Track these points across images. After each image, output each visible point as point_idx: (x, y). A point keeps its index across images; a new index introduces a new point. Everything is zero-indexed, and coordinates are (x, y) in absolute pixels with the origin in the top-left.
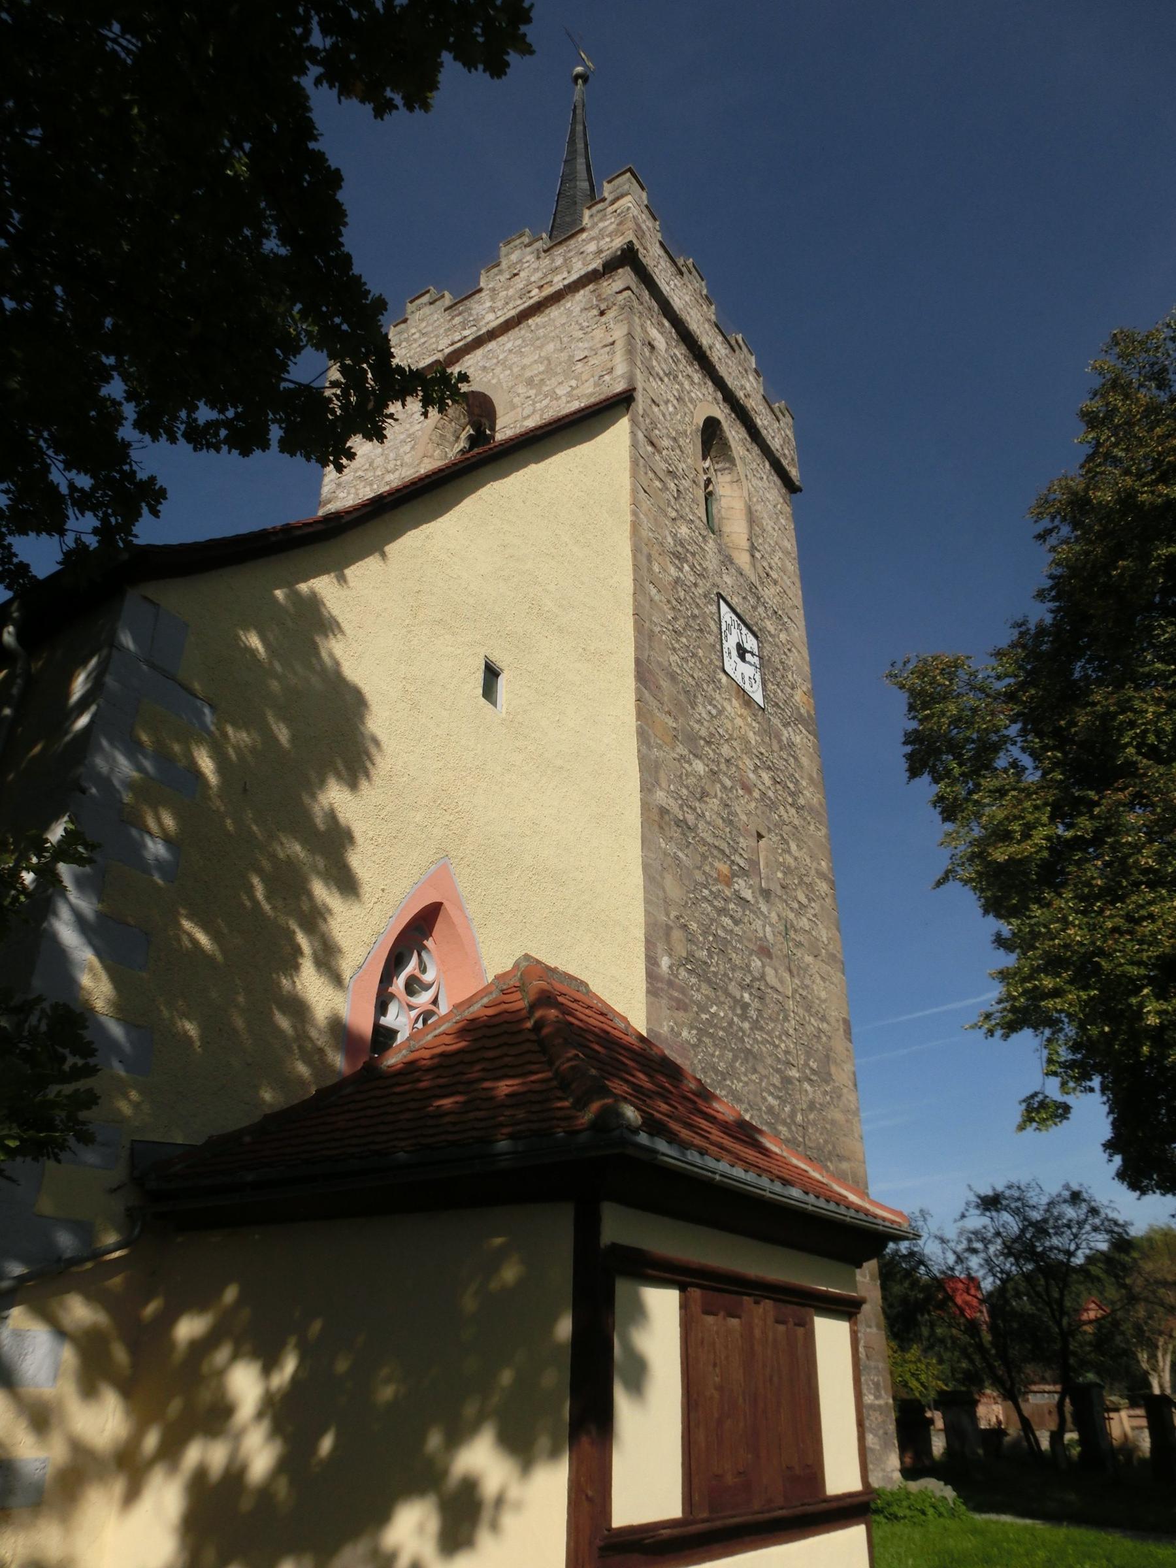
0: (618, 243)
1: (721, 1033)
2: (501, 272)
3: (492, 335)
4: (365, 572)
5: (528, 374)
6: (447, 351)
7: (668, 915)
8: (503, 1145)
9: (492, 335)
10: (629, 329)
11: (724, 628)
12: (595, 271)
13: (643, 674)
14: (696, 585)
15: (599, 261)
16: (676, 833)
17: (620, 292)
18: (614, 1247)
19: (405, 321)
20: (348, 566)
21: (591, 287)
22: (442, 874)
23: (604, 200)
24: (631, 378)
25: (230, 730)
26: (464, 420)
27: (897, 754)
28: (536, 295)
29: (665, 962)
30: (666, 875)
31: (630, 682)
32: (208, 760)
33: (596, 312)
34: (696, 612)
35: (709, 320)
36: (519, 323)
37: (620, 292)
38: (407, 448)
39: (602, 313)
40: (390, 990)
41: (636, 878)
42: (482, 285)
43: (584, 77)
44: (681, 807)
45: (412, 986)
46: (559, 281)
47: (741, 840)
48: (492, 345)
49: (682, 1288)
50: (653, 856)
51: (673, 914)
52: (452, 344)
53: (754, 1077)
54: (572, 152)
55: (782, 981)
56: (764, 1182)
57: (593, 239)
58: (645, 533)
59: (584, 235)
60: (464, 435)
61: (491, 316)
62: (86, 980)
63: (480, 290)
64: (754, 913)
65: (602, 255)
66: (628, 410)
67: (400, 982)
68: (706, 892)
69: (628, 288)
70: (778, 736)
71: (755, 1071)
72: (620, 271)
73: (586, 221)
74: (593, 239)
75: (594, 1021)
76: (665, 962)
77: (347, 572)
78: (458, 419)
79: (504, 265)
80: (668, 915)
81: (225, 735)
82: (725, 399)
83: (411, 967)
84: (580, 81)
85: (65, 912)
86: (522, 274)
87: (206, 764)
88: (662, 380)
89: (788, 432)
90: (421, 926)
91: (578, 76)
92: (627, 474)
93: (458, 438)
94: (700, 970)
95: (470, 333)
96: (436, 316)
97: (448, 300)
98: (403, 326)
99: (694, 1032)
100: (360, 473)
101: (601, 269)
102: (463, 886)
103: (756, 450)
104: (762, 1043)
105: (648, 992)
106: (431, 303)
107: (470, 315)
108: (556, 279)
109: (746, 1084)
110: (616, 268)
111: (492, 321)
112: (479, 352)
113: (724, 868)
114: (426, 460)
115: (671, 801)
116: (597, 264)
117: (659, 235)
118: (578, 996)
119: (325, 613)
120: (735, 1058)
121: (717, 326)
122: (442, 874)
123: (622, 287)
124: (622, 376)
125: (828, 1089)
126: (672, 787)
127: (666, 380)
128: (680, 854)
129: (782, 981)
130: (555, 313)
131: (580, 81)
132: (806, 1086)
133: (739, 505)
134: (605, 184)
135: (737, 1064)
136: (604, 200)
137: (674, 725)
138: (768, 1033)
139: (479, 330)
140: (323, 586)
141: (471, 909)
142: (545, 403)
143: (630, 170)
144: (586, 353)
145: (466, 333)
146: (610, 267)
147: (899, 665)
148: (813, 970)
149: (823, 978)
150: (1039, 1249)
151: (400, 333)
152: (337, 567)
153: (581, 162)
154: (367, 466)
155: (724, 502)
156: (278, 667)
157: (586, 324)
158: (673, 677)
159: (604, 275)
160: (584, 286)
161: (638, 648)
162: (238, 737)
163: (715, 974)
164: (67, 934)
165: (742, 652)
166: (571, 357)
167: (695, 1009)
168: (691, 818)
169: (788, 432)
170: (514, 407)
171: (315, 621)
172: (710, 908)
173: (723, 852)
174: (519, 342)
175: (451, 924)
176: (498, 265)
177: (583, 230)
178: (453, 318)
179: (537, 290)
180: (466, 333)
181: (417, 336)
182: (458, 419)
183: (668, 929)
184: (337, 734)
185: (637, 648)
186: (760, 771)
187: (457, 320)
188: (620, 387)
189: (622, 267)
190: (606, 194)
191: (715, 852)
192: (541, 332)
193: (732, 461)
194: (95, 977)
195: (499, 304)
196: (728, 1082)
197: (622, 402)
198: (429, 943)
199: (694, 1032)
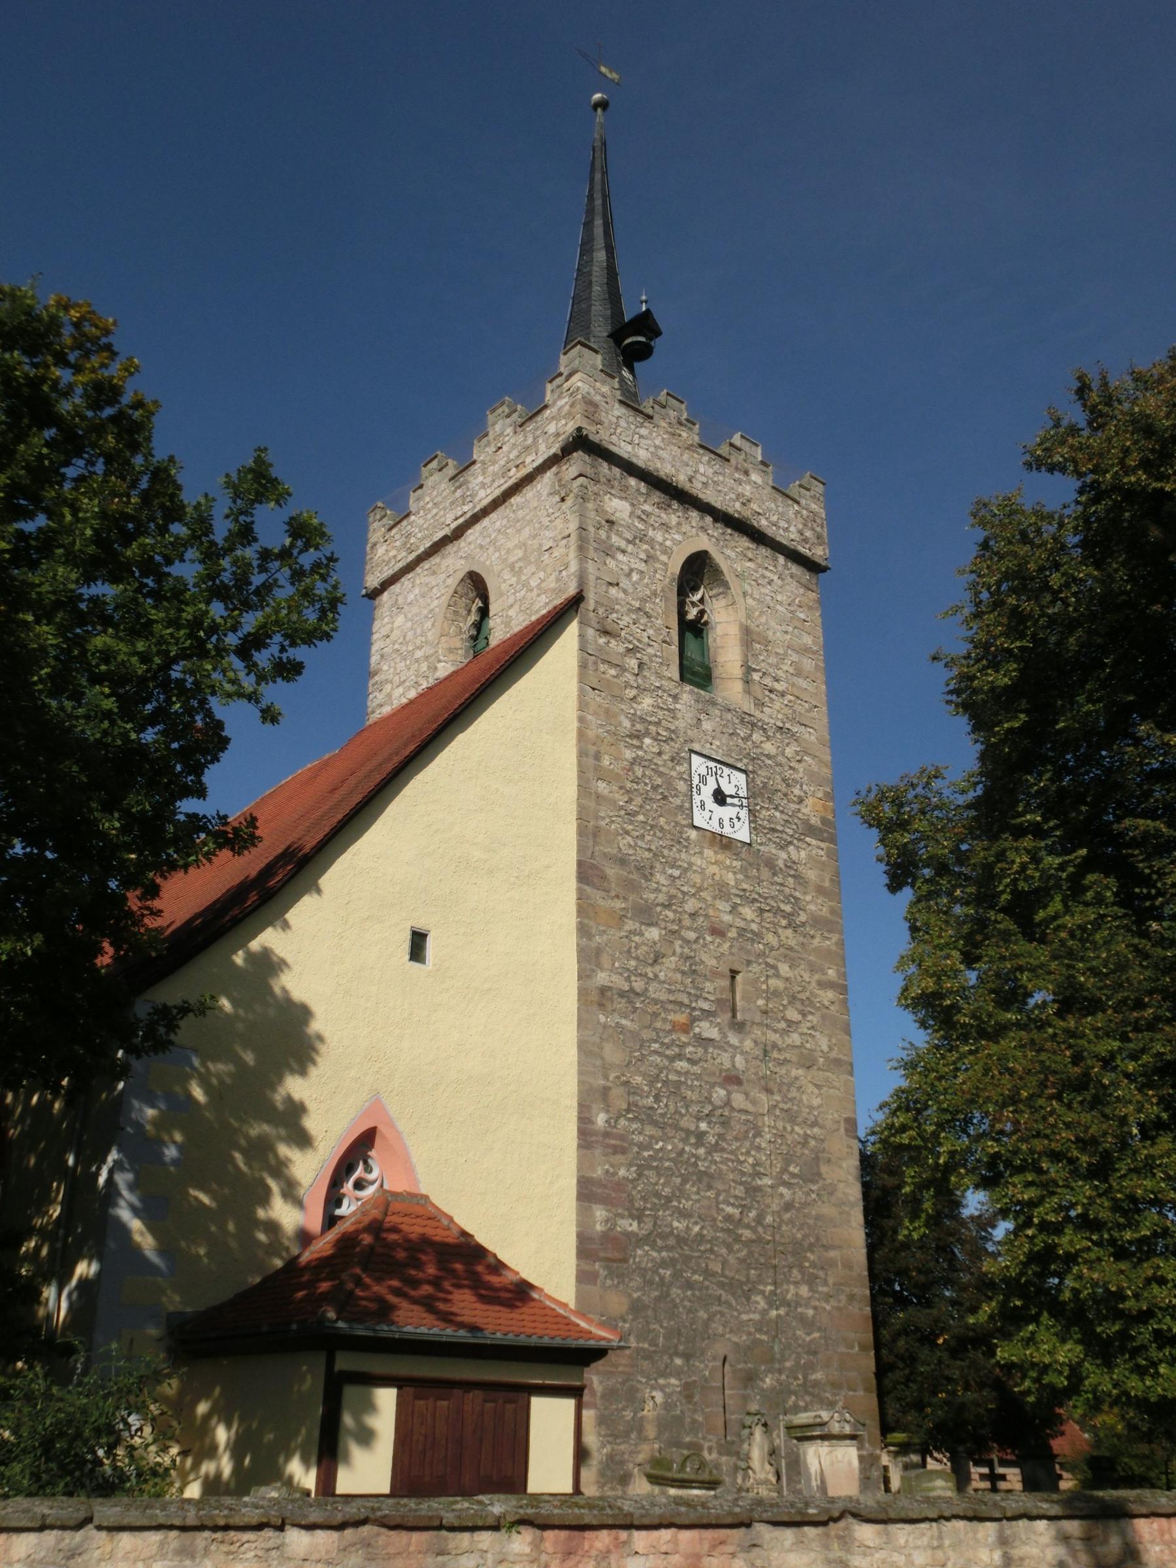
0: (570, 428)
1: (667, 1164)
2: (488, 444)
3: (485, 512)
4: (304, 912)
5: (512, 559)
6: (453, 526)
7: (606, 1077)
8: (294, 1327)
9: (485, 512)
10: (581, 522)
11: (696, 781)
12: (555, 455)
13: (587, 873)
14: (660, 754)
15: (557, 445)
16: (621, 1004)
17: (575, 478)
18: (341, 1372)
19: (421, 487)
20: (287, 911)
21: (554, 469)
22: (376, 1105)
23: (561, 374)
24: (582, 578)
25: (210, 1065)
26: (472, 595)
27: (879, 875)
28: (516, 475)
29: (601, 1119)
30: (605, 1044)
31: (572, 884)
32: (198, 1090)
33: (557, 498)
34: (659, 781)
35: (689, 448)
36: (504, 501)
37: (575, 478)
38: (429, 624)
39: (563, 500)
40: (342, 1191)
41: (570, 1055)
42: (475, 457)
43: (603, 105)
44: (628, 979)
45: (359, 1185)
46: (532, 461)
47: (708, 984)
48: (486, 522)
49: (399, 1388)
50: (591, 1033)
51: (612, 1077)
52: (456, 519)
53: (708, 1194)
54: (590, 212)
55: (754, 1102)
56: (462, 1333)
57: (553, 418)
58: (591, 734)
59: (547, 413)
60: (474, 608)
61: (482, 493)
62: (137, 1238)
63: (474, 462)
64: (720, 1048)
65: (560, 439)
66: (577, 611)
67: (349, 1185)
68: (655, 1046)
69: (581, 475)
70: (770, 864)
71: (710, 1187)
72: (575, 454)
73: (548, 397)
74: (553, 418)
75: (415, 1229)
76: (601, 1119)
77: (288, 916)
78: (467, 594)
79: (491, 436)
80: (606, 1077)
81: (207, 1069)
82: (716, 520)
83: (359, 1172)
84: (599, 110)
85: (122, 1203)
86: (505, 448)
87: (198, 1093)
88: (624, 552)
89: (814, 506)
90: (361, 1147)
91: (597, 105)
92: (575, 679)
93: (469, 611)
94: (648, 1117)
95: (469, 509)
96: (443, 486)
97: (451, 471)
98: (420, 491)
99: (634, 1169)
100: (396, 646)
101: (559, 453)
102: (393, 1109)
103: (764, 551)
104: (721, 1162)
105: (580, 1146)
106: (440, 470)
107: (468, 489)
108: (528, 460)
109: (698, 1201)
110: (570, 453)
111: (484, 497)
112: (478, 527)
113: (681, 1018)
114: (443, 639)
115: (615, 978)
116: (555, 449)
117: (618, 393)
118: (421, 1211)
119: (275, 959)
120: (685, 1181)
121: (701, 446)
122: (376, 1105)
123: (576, 474)
124: (574, 574)
125: (814, 1188)
126: (617, 964)
127: (630, 548)
128: (624, 1022)
129: (754, 1102)
130: (529, 493)
131: (599, 110)
132: (782, 1189)
133: (734, 631)
134: (562, 356)
135: (688, 1186)
136: (561, 374)
137: (623, 905)
138: (732, 1152)
139: (474, 507)
140: (268, 939)
141: (401, 1126)
142: (523, 593)
143: (580, 343)
144: (551, 544)
145: (466, 508)
146: (567, 450)
147: (864, 793)
148: (803, 1081)
149: (818, 1086)
150: (665, 1357)
151: (418, 499)
152: (277, 919)
153: (598, 222)
154: (401, 640)
155: (719, 630)
156: (241, 1012)
157: (551, 511)
158: (622, 861)
159: (563, 457)
160: (550, 468)
161: (581, 849)
162: (219, 1068)
163: (663, 1115)
164: (124, 1214)
165: (720, 797)
166: (541, 545)
167: (636, 1149)
168: (638, 985)
169: (814, 506)
170: (502, 595)
171: (267, 964)
172: (659, 1059)
173: (681, 1004)
174: (505, 522)
175: (384, 1138)
176: (486, 435)
177: (546, 407)
178: (455, 491)
179: (514, 470)
180: (466, 508)
181: (430, 505)
182: (467, 594)
183: (606, 1090)
184: (290, 1038)
185: (579, 851)
186: (740, 909)
187: (459, 493)
188: (572, 591)
189: (576, 450)
190: (562, 369)
191: (670, 1007)
192: (520, 513)
193: (726, 585)
194: (142, 1234)
195: (488, 480)
196: (675, 1203)
197: (574, 604)
198: (372, 1153)
199: (634, 1169)
